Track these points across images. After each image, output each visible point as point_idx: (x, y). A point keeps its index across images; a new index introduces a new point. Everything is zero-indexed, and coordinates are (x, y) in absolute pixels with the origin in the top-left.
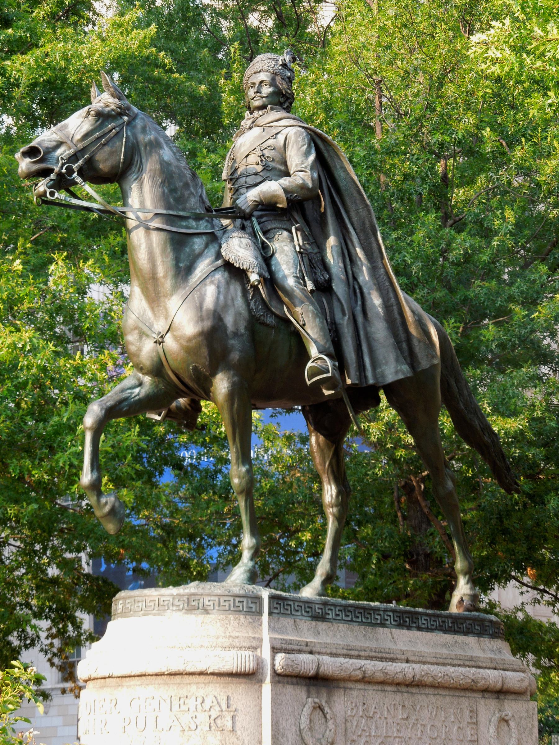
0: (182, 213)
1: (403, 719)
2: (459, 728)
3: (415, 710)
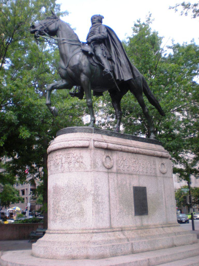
1: (134, 162)
2: (150, 165)
3: (137, 159)
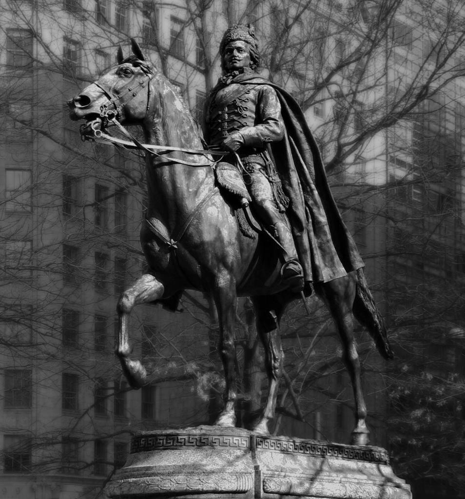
0: (190, 151)
